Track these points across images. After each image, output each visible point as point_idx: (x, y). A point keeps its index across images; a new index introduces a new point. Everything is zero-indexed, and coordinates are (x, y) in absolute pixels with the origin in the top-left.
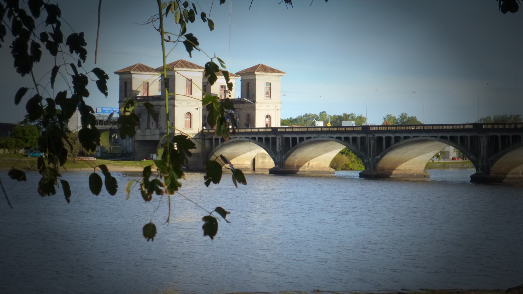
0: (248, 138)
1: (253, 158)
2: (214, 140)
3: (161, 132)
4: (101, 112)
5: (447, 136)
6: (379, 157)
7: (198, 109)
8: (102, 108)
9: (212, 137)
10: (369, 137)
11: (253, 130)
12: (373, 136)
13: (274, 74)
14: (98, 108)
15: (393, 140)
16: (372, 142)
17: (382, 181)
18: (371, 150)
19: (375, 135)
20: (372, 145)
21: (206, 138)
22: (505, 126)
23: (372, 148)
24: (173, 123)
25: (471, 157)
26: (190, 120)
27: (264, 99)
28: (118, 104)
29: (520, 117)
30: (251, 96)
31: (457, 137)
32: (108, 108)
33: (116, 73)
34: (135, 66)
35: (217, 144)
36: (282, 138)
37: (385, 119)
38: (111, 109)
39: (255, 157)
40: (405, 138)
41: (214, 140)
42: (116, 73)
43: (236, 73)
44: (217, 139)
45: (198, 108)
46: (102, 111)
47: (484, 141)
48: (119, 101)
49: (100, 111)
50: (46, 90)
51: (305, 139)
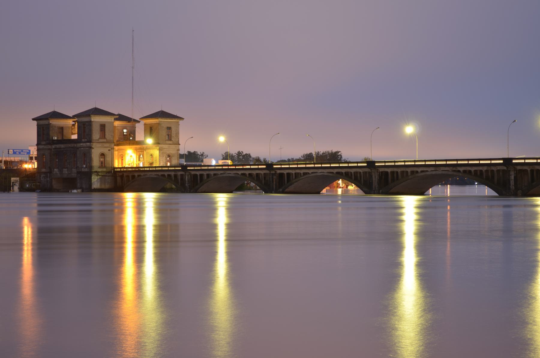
3: (78, 171)
4: (12, 153)
7: (111, 150)
8: (13, 150)
10: (272, 174)
14: (10, 150)
16: (274, 177)
18: (273, 184)
20: (274, 180)
21: (117, 175)
23: (274, 183)
25: (364, 189)
26: (104, 160)
29: (339, 154)
32: (18, 150)
33: (33, 119)
37: (223, 156)
38: (21, 151)
41: (125, 177)
42: (33, 119)
43: (73, 115)
46: (13, 153)
48: (37, 144)
49: (11, 152)
50: (281, 147)
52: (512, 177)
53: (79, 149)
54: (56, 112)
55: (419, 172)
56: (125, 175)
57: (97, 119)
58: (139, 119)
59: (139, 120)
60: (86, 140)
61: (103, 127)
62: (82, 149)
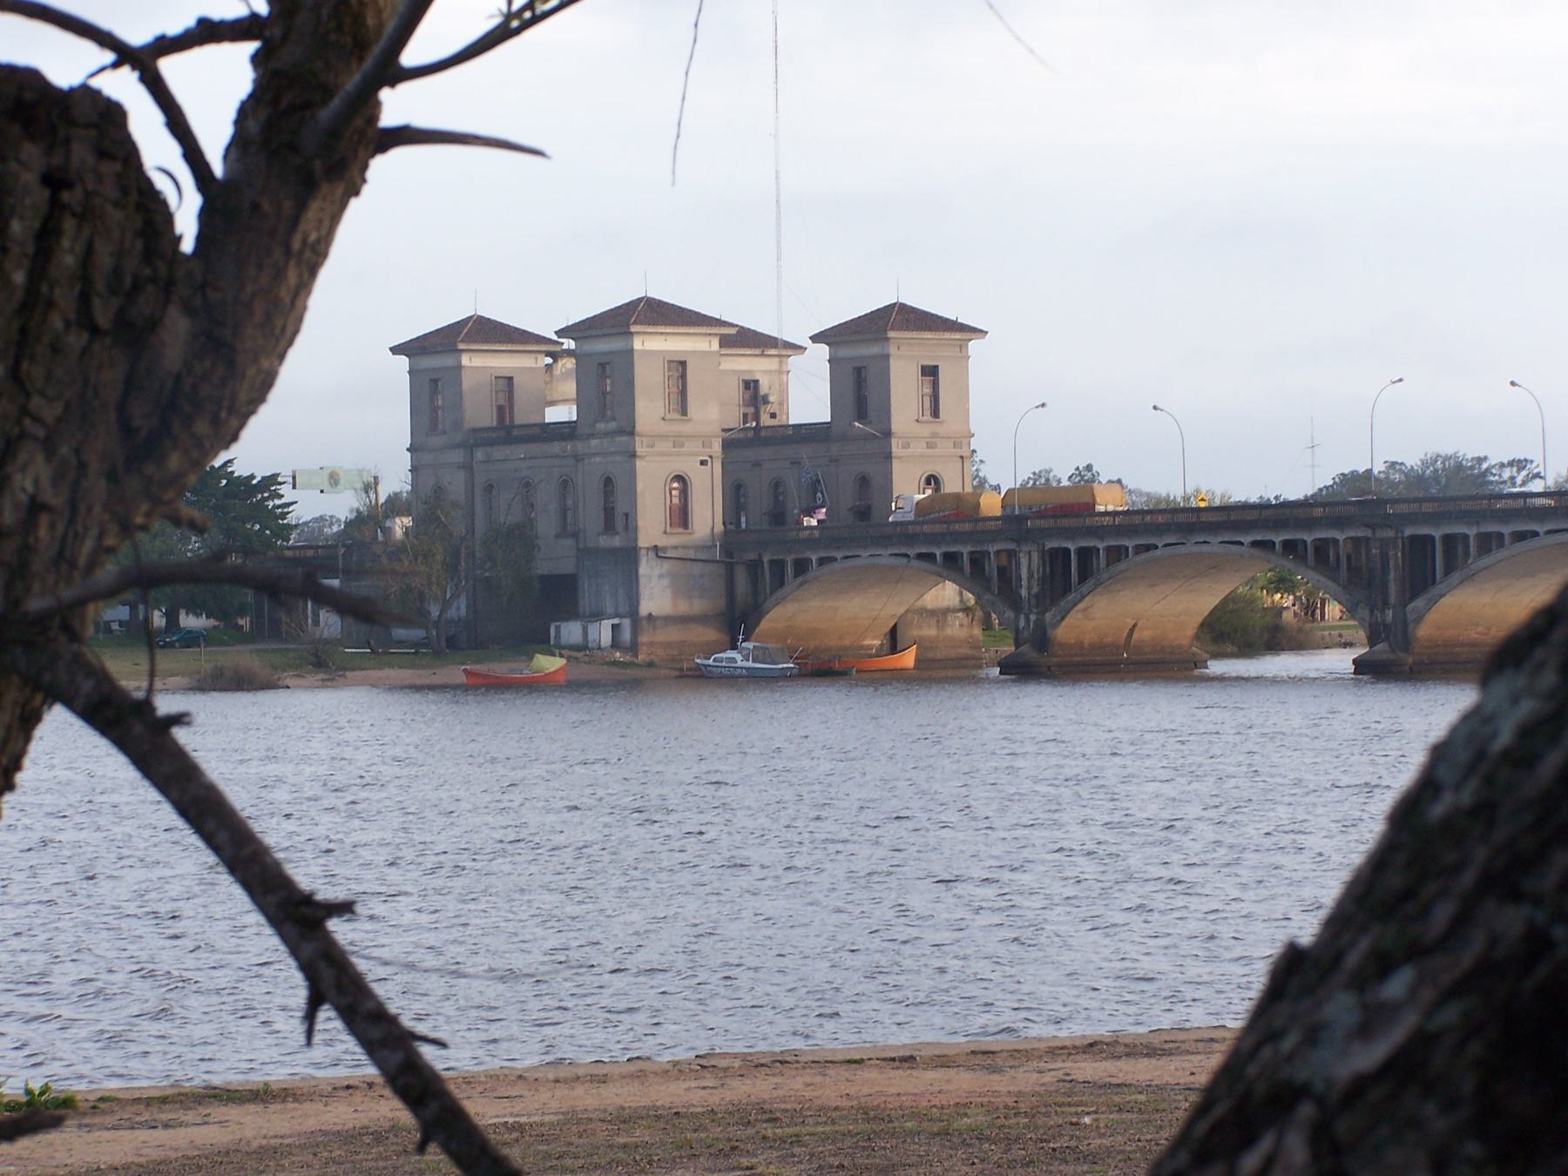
0: (906, 556)
1: (892, 624)
2: (766, 566)
5: (1434, 534)
6: (1419, 603)
7: (709, 464)
9: (760, 555)
10: (1381, 540)
11: (1088, 522)
12: (1397, 533)
13: (947, 335)
15: (790, 570)
17: (1408, 684)
19: (1402, 532)
22: (1525, 502)
24: (627, 515)
27: (917, 421)
28: (409, 454)
30: (872, 414)
31: (1432, 538)
33: (396, 350)
34: (468, 323)
35: (779, 582)
36: (1043, 553)
39: (896, 625)
40: (1520, 537)
41: (766, 566)
42: (396, 350)
44: (778, 566)
45: (709, 459)
47: (1028, 565)
51: (1507, 540)
52: (310, 620)
53: (586, 461)
54: (481, 318)
55: (1160, 546)
56: (765, 560)
57: (650, 344)
58: (556, 332)
59: (555, 337)
60: (613, 425)
61: (680, 367)
62: (598, 459)
